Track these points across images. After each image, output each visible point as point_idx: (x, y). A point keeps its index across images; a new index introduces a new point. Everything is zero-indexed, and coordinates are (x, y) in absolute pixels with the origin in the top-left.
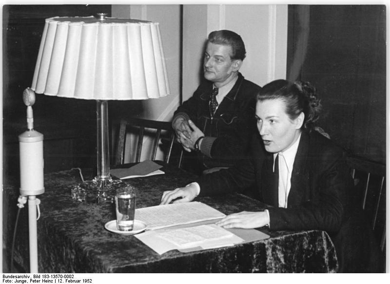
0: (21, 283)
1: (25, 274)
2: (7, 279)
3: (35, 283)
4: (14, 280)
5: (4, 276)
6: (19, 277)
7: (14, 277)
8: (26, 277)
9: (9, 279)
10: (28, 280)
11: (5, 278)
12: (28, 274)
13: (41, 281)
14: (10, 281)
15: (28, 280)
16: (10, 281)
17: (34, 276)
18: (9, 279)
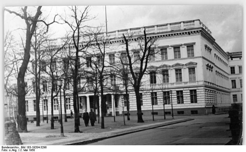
0: (14, 151)
1: (16, 146)
2: (4, 149)
3: (5, 151)
5: (2, 147)
6: (12, 148)
7: (9, 147)
8: (16, 148)
9: (6, 149)
10: (17, 149)
11: (3, 148)
12: (18, 146)
13: (29, 150)
17: (22, 147)
18: (6, 149)
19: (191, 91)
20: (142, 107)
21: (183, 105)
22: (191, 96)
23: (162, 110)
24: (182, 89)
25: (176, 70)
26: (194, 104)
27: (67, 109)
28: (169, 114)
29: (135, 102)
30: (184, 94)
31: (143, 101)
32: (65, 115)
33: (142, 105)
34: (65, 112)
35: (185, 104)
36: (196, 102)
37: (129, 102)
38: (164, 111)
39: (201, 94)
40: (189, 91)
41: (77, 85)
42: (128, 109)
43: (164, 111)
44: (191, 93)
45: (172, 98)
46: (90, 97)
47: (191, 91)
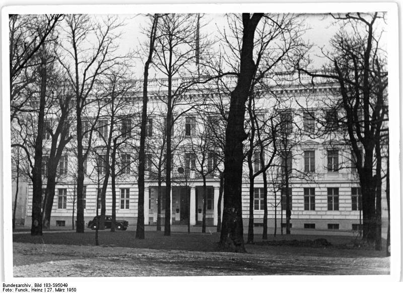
0: (6, 284)
2: (7, 288)
3: (8, 292)
4: (14, 288)
5: (4, 285)
6: (20, 286)
7: (14, 286)
8: (27, 286)
9: (10, 288)
11: (5, 287)
13: (66, 290)
14: (11, 290)
15: (29, 289)
16: (11, 290)
18: (10, 288)
19: (330, 190)
20: (85, 211)
21: (313, 213)
22: (306, 199)
23: (70, 217)
24: (338, 185)
25: (306, 152)
26: (333, 212)
27: (257, 208)
28: (334, 228)
29: (341, 199)
30: (340, 193)
31: (87, 201)
32: (251, 219)
33: (85, 208)
34: (251, 214)
35: (341, 211)
36: (337, 208)
37: (291, 199)
38: (282, 221)
39: (323, 195)
40: (303, 190)
41: (380, 150)
42: (289, 214)
43: (282, 221)
44: (305, 194)
45: (74, 203)
46: (197, 188)
47: (330, 190)
